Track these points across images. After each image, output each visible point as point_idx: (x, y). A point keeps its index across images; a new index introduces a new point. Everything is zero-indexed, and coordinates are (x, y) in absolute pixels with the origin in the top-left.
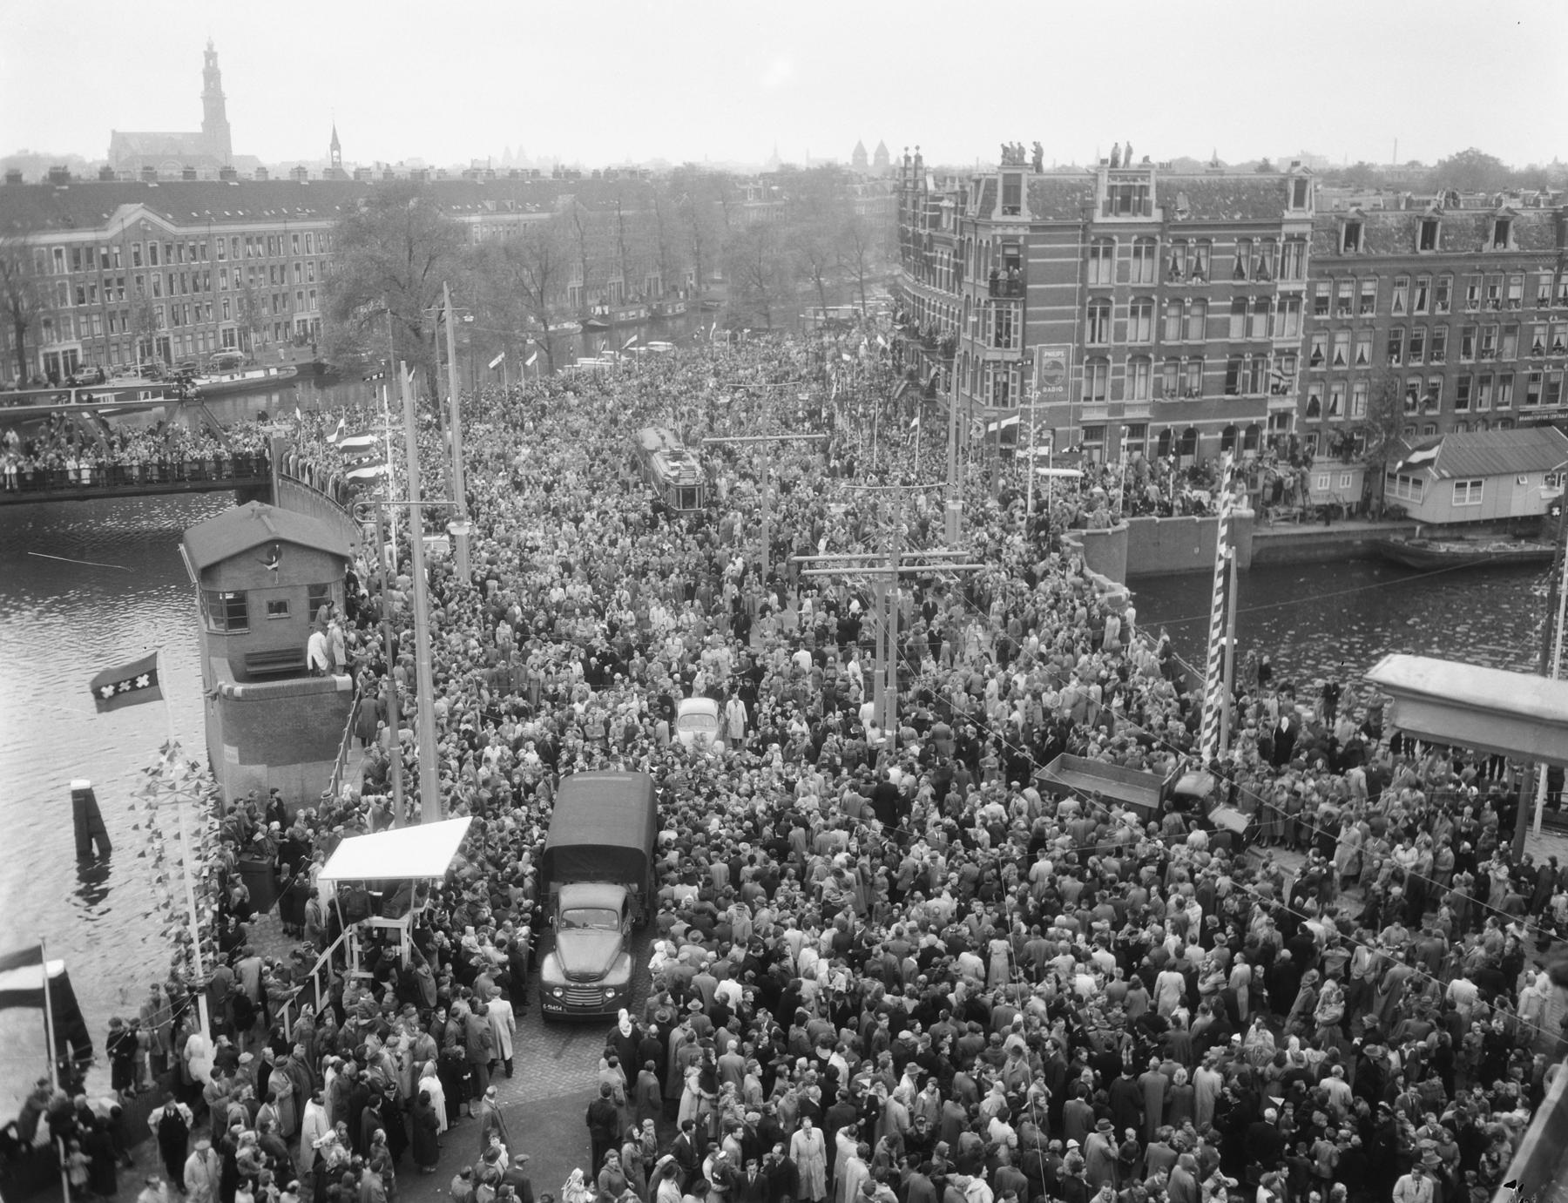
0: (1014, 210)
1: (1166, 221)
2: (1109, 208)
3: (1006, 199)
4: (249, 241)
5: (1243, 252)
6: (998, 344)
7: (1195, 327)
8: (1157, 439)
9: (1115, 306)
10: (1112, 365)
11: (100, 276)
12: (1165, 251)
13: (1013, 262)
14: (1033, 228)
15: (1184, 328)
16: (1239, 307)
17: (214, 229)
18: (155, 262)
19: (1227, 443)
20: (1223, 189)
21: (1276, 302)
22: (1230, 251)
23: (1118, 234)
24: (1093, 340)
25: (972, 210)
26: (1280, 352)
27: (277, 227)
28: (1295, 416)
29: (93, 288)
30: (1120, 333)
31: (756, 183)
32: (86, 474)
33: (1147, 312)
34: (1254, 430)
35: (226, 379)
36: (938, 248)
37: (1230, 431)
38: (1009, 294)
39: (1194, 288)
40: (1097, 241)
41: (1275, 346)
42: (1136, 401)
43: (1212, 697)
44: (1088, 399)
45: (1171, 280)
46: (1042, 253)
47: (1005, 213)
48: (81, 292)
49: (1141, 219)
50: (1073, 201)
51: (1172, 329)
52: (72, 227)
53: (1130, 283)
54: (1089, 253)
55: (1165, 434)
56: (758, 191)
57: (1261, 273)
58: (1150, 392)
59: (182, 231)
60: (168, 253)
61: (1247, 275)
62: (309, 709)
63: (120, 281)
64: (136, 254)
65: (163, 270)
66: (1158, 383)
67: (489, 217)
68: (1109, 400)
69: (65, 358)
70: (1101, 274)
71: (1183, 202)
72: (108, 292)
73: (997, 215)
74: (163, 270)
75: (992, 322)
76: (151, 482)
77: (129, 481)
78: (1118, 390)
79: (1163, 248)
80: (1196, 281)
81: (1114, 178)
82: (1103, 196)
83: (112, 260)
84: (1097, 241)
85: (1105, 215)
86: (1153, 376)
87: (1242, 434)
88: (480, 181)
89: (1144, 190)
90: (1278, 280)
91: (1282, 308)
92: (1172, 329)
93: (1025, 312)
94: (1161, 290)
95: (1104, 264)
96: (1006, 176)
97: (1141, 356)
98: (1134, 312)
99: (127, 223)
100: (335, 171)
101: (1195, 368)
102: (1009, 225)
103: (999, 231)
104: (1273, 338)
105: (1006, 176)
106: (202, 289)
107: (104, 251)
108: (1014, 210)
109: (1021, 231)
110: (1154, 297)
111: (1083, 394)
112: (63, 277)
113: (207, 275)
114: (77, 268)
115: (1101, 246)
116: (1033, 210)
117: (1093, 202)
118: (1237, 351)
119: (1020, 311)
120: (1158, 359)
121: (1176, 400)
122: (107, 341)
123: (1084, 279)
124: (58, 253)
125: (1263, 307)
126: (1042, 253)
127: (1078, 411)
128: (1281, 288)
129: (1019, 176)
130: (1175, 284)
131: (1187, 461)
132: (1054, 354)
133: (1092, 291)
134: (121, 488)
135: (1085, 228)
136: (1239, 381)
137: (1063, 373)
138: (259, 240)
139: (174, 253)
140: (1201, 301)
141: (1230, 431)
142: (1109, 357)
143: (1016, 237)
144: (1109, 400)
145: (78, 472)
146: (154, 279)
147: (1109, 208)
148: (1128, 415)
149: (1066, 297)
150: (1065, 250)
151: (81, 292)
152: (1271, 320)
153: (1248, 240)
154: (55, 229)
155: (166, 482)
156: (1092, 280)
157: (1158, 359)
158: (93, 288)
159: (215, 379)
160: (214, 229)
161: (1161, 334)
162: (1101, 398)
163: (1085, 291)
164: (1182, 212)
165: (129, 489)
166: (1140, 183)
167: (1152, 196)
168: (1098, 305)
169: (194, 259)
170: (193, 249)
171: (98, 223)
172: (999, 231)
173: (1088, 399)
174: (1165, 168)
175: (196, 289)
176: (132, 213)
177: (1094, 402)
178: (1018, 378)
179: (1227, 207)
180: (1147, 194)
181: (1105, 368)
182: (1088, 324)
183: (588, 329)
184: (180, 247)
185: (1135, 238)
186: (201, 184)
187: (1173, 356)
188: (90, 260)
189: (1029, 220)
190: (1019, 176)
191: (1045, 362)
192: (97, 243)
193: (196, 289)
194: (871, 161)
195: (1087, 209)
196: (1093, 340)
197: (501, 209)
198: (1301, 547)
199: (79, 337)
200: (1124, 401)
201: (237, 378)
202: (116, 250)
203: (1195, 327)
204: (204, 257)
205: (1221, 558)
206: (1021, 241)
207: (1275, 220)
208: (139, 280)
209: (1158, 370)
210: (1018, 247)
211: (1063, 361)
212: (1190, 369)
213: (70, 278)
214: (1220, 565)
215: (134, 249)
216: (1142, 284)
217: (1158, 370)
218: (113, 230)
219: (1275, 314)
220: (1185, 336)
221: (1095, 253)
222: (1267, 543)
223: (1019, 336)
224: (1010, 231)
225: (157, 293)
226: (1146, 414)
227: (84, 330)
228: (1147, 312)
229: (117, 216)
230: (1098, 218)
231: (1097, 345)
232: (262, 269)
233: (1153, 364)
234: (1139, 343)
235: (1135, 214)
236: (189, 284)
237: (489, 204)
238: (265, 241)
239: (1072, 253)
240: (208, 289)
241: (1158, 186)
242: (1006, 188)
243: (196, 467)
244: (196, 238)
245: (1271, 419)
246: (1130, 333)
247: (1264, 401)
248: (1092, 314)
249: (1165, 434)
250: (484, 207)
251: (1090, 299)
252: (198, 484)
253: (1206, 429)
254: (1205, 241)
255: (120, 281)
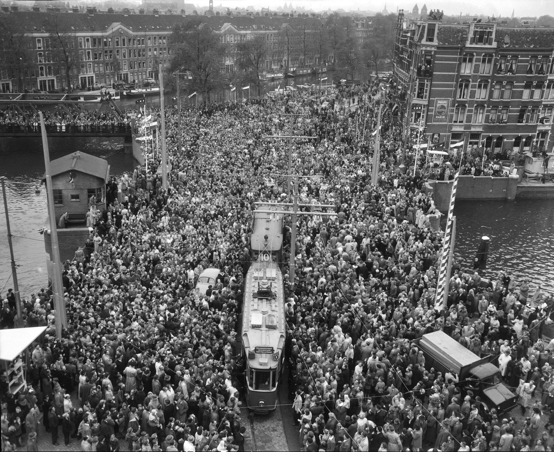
0: (431, 40)
1: (498, 46)
2: (473, 41)
3: (428, 35)
4: (160, 38)
5: (533, 62)
6: (418, 97)
7: (507, 93)
8: (485, 140)
9: (471, 83)
10: (467, 108)
11: (103, 49)
12: (496, 61)
13: (429, 62)
14: (438, 48)
15: (502, 95)
16: (527, 86)
17: (147, 33)
18: (124, 45)
19: (516, 144)
20: (527, 34)
21: (546, 84)
22: (527, 61)
23: (475, 52)
24: (460, 98)
25: (416, 38)
26: (545, 106)
27: (143, 33)
28: (550, 133)
29: (100, 54)
30: (473, 94)
31: (363, 21)
32: (64, 128)
33: (485, 87)
34: (529, 139)
35: (144, 90)
36: (405, 53)
37: (518, 139)
38: (425, 76)
39: (508, 77)
40: (466, 55)
41: (543, 103)
42: (477, 124)
43: (441, 282)
44: (455, 122)
45: (499, 73)
46: (441, 59)
47: (427, 41)
48: (96, 55)
49: (487, 46)
50: (457, 37)
51: (496, 93)
52: (93, 30)
53: (479, 74)
54: (462, 60)
55: (489, 139)
56: (363, 24)
57: (541, 71)
58: (484, 120)
59: (135, 33)
60: (129, 42)
61: (534, 72)
62: (78, 241)
63: (111, 52)
64: (117, 42)
65: (127, 48)
66: (487, 117)
67: (254, 32)
68: (464, 123)
69: (89, 79)
70: (467, 70)
71: (507, 39)
72: (106, 55)
73: (424, 41)
74: (127, 48)
75: (417, 87)
76: (88, 132)
77: (80, 131)
78: (469, 119)
79: (496, 59)
80: (509, 74)
81: (477, 28)
82: (471, 35)
83: (108, 43)
84: (466, 55)
85: (471, 43)
86: (485, 114)
87: (524, 140)
88: (261, 15)
89: (490, 33)
90: (548, 74)
91: (549, 87)
92: (496, 93)
93: (431, 84)
94: (493, 77)
95: (469, 65)
96: (429, 24)
97: (481, 105)
98: (480, 86)
99: (114, 30)
100: (211, 10)
101: (505, 111)
102: (428, 46)
103: (424, 48)
104: (543, 100)
105: (429, 24)
106: (141, 56)
107: (105, 40)
108: (431, 40)
109: (433, 49)
110: (489, 80)
111: (454, 119)
112: (89, 49)
113: (144, 50)
114: (94, 46)
115: (467, 57)
116: (439, 40)
117: (467, 38)
118: (525, 105)
119: (429, 83)
120: (488, 107)
121: (495, 124)
122: (105, 74)
123: (459, 71)
124: (88, 40)
125: (540, 86)
126: (441, 59)
127: (451, 127)
128: (549, 78)
129: (435, 25)
130: (500, 75)
131: (497, 150)
132: (442, 102)
133: (461, 76)
134: (76, 134)
135: (461, 49)
136: (525, 117)
137: (446, 110)
138: (164, 38)
139: (131, 41)
140: (510, 83)
141: (518, 139)
142: (467, 105)
143: (431, 51)
144: (464, 123)
145: (61, 127)
146: (123, 52)
147: (473, 41)
148: (473, 129)
149: (450, 78)
150: (451, 58)
151: (96, 55)
152: (543, 92)
153: (535, 57)
154: (87, 31)
155: (93, 132)
156: (462, 71)
157: (488, 107)
158: (100, 54)
159: (140, 90)
160: (147, 33)
161: (491, 95)
162: (461, 122)
163: (459, 76)
164: (506, 44)
165: (79, 134)
166: (488, 30)
167: (493, 36)
168: (464, 82)
169: (139, 44)
170: (139, 40)
171: (104, 29)
172: (424, 48)
173: (455, 122)
174: (505, 22)
175: (139, 56)
176: (117, 26)
177: (458, 124)
178: (426, 112)
179: (527, 42)
180: (491, 35)
181: (464, 109)
182: (459, 90)
183: (287, 76)
184: (134, 40)
185: (483, 54)
186: (146, 16)
187: (495, 106)
188: (99, 43)
189: (437, 44)
190: (435, 25)
191: (438, 105)
192: (103, 36)
193: (139, 56)
194: (420, 12)
195: (464, 40)
196: (460, 98)
197: (259, 28)
198: (539, 192)
199: (94, 72)
200: (471, 123)
201: (148, 90)
202: (110, 40)
203: (507, 93)
204: (143, 44)
205: (450, 220)
206: (433, 53)
207: (550, 48)
208: (118, 51)
209: (488, 111)
210: (431, 55)
211: (446, 105)
212: (503, 111)
213: (92, 50)
214: (449, 223)
215: (116, 40)
216: (485, 74)
217: (488, 111)
218: (109, 32)
219: (545, 89)
220: (502, 98)
221: (465, 60)
222: (524, 190)
223: (428, 94)
224: (428, 49)
225: (124, 57)
226: (481, 129)
227: (96, 69)
228: (485, 87)
229: (110, 28)
230: (468, 45)
231: (462, 99)
232: (165, 49)
233: (486, 109)
234: (481, 100)
235: (485, 44)
236: (137, 54)
237: (254, 26)
238: (167, 38)
239: (455, 59)
240: (144, 56)
241: (497, 31)
242: (428, 30)
243: (104, 128)
244: (141, 36)
245: (538, 134)
246: (477, 96)
247: (536, 126)
248: (461, 86)
249: (489, 139)
250: (253, 27)
251: (460, 79)
252: (105, 134)
253: (507, 137)
254: (515, 57)
255: (111, 52)
